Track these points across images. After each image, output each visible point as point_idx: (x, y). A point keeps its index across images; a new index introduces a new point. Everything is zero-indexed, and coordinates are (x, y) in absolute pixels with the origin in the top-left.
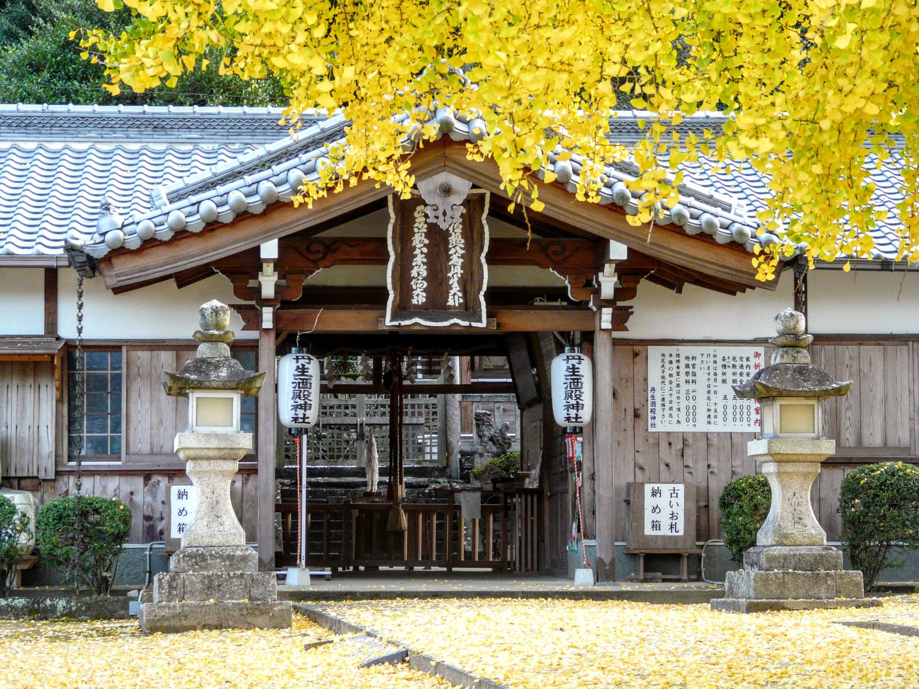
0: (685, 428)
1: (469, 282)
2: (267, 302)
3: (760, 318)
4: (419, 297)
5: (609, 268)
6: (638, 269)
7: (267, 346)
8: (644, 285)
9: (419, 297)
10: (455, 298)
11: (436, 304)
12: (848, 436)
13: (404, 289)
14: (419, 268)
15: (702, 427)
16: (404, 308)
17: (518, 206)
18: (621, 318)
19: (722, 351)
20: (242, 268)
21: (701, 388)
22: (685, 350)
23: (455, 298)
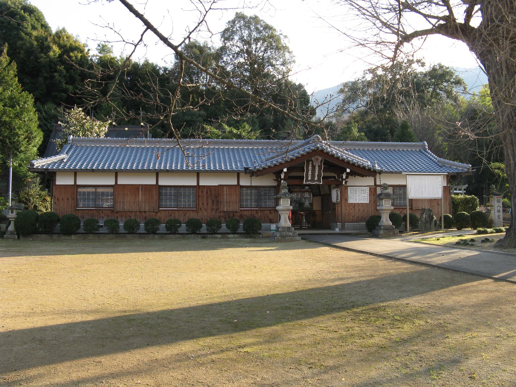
0: (355, 202)
1: (319, 176)
2: (282, 179)
3: (369, 181)
4: (310, 178)
5: (283, 173)
6: (353, 173)
8: (350, 177)
9: (310, 178)
10: (316, 179)
11: (313, 179)
12: (77, 317)
13: (307, 177)
15: (358, 202)
16: (307, 180)
17: (18, 141)
18: (346, 183)
19: (361, 188)
20: (278, 173)
21: (357, 194)
22: (355, 188)
23: (316, 179)
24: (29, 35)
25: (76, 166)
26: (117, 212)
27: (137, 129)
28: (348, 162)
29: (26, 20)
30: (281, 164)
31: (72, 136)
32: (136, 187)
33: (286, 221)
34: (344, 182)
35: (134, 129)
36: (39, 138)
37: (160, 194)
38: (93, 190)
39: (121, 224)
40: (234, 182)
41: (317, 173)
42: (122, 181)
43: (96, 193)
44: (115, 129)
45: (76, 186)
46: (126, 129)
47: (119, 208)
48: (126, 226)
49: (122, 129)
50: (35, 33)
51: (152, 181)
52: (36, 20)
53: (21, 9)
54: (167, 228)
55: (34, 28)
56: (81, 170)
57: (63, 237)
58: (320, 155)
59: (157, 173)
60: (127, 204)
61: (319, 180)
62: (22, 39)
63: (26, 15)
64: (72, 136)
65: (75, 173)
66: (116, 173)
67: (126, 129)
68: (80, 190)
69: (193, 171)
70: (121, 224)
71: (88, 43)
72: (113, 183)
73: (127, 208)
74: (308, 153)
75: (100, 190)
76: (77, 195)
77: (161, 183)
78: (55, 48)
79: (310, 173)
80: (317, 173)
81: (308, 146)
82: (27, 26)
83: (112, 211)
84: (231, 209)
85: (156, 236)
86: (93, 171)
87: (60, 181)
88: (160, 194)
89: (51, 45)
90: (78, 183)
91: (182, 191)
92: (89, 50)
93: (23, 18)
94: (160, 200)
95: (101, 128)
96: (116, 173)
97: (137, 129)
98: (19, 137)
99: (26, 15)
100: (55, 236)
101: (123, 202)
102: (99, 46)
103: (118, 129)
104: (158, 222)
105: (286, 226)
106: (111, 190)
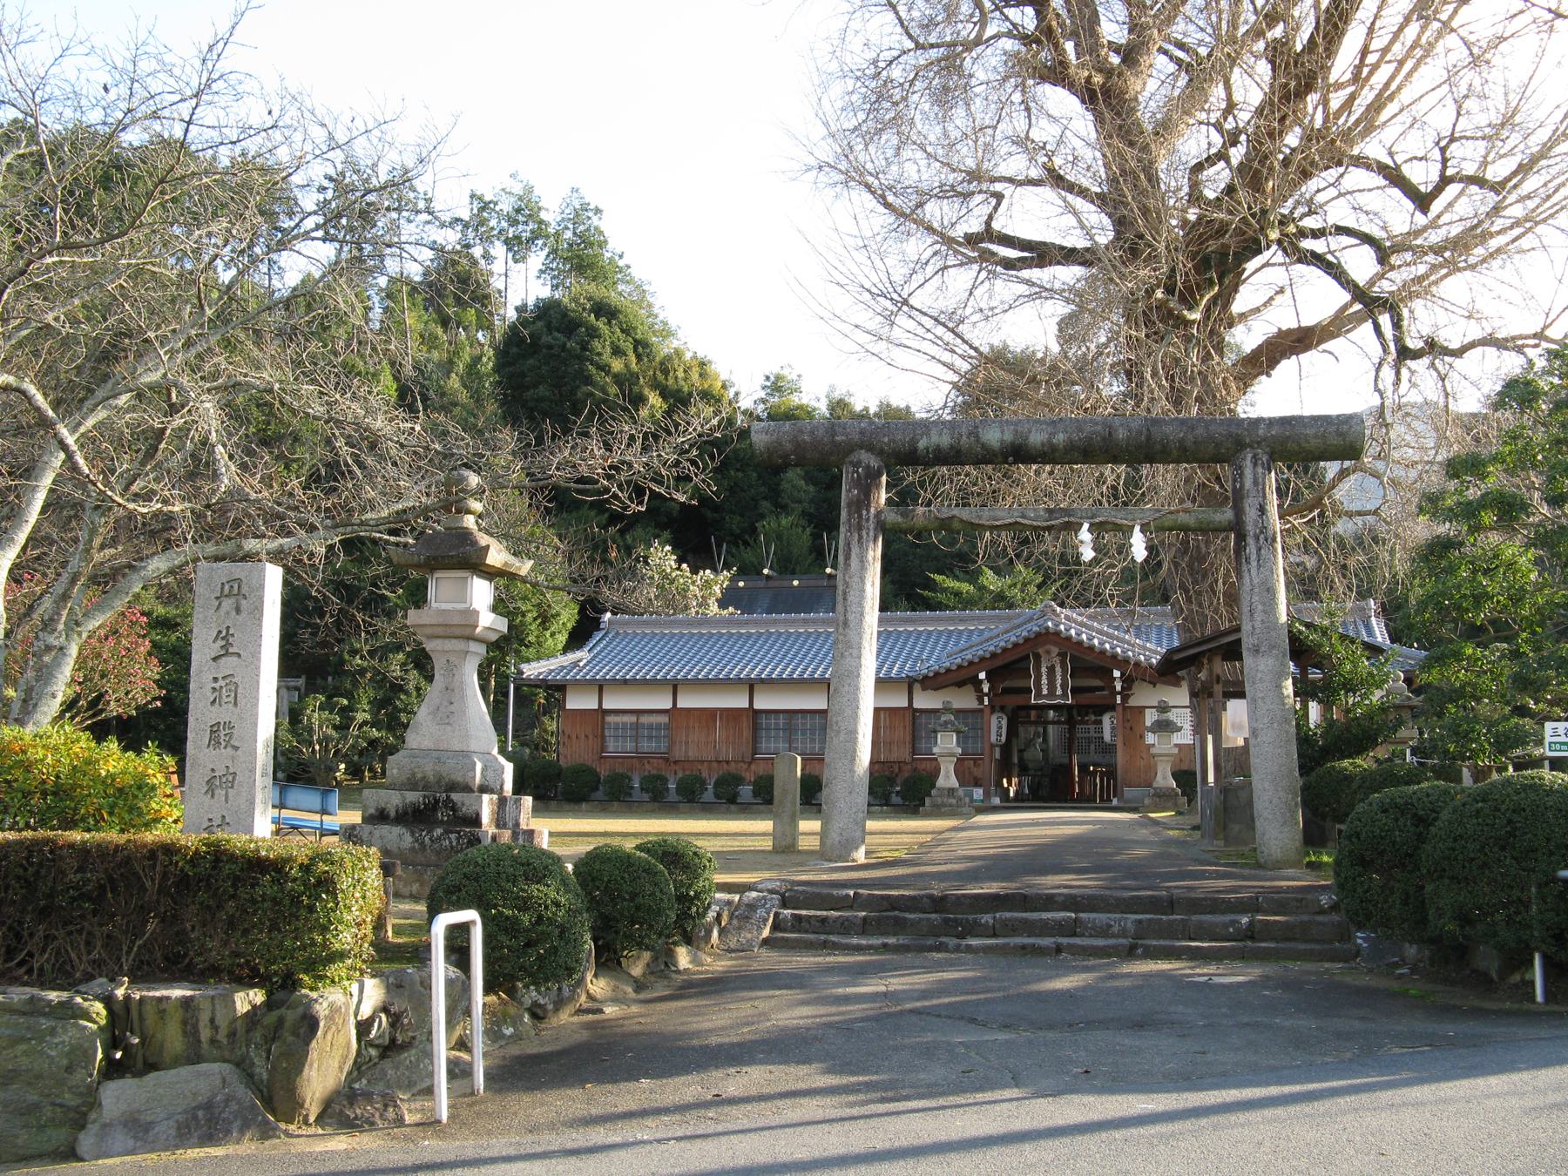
4: (1045, 692)
7: (987, 711)
9: (1045, 692)
10: (1059, 692)
13: (1039, 690)
14: (1044, 681)
16: (1039, 695)
23: (1059, 692)
24: (604, 368)
25: (814, 672)
26: (675, 762)
27: (820, 583)
28: (971, 663)
29: (599, 337)
30: (1114, 656)
31: (608, 615)
32: (711, 714)
33: (948, 777)
34: (1119, 699)
35: (812, 583)
36: (568, 616)
37: (756, 728)
38: (633, 719)
39: (672, 786)
40: (902, 702)
41: (1059, 682)
42: (685, 702)
43: (637, 726)
44: (771, 584)
45: (603, 712)
46: (796, 583)
47: (678, 754)
48: (680, 789)
49: (786, 583)
50: (617, 365)
51: (740, 702)
52: (623, 331)
53: (591, 311)
54: (756, 794)
55: (617, 352)
56: (685, 681)
57: (566, 806)
58: (1055, 644)
59: (752, 686)
60: (693, 747)
61: (1065, 695)
62: (588, 380)
63: (601, 324)
64: (608, 615)
65: (601, 687)
66: (601, 687)
67: (796, 583)
68: (610, 719)
69: (592, 682)
70: (672, 786)
71: (734, 379)
72: (669, 706)
73: (693, 754)
74: (1027, 640)
75: (645, 719)
76: (603, 729)
77: (759, 704)
78: (654, 399)
79: (1044, 681)
80: (1059, 682)
81: (1028, 626)
82: (603, 348)
83: (667, 760)
84: (894, 757)
85: (733, 807)
86: (625, 682)
87: (575, 702)
88: (756, 728)
89: (646, 391)
90: (606, 706)
91: (799, 720)
92: (737, 394)
93: (593, 333)
94: (755, 739)
95: (708, 587)
96: (675, 687)
97: (820, 583)
98: (524, 616)
99: (601, 324)
100: (553, 804)
101: (687, 743)
102: (768, 378)
103: (777, 584)
104: (738, 780)
105: (948, 786)
106: (664, 719)
